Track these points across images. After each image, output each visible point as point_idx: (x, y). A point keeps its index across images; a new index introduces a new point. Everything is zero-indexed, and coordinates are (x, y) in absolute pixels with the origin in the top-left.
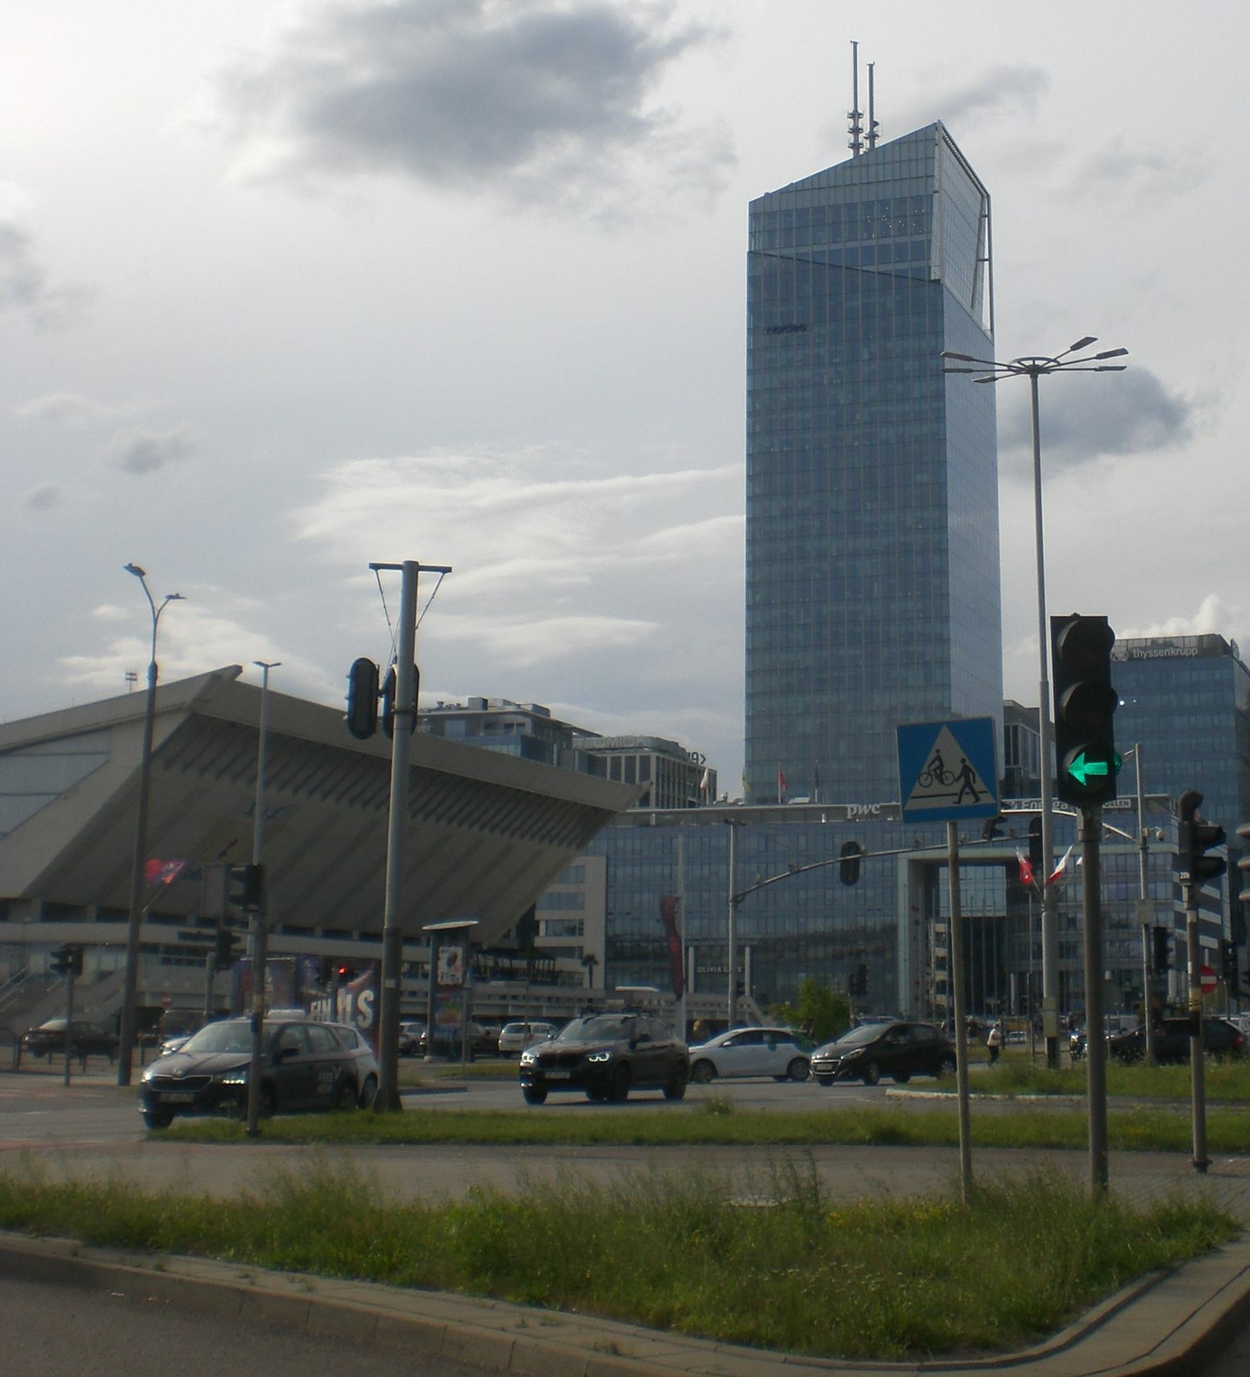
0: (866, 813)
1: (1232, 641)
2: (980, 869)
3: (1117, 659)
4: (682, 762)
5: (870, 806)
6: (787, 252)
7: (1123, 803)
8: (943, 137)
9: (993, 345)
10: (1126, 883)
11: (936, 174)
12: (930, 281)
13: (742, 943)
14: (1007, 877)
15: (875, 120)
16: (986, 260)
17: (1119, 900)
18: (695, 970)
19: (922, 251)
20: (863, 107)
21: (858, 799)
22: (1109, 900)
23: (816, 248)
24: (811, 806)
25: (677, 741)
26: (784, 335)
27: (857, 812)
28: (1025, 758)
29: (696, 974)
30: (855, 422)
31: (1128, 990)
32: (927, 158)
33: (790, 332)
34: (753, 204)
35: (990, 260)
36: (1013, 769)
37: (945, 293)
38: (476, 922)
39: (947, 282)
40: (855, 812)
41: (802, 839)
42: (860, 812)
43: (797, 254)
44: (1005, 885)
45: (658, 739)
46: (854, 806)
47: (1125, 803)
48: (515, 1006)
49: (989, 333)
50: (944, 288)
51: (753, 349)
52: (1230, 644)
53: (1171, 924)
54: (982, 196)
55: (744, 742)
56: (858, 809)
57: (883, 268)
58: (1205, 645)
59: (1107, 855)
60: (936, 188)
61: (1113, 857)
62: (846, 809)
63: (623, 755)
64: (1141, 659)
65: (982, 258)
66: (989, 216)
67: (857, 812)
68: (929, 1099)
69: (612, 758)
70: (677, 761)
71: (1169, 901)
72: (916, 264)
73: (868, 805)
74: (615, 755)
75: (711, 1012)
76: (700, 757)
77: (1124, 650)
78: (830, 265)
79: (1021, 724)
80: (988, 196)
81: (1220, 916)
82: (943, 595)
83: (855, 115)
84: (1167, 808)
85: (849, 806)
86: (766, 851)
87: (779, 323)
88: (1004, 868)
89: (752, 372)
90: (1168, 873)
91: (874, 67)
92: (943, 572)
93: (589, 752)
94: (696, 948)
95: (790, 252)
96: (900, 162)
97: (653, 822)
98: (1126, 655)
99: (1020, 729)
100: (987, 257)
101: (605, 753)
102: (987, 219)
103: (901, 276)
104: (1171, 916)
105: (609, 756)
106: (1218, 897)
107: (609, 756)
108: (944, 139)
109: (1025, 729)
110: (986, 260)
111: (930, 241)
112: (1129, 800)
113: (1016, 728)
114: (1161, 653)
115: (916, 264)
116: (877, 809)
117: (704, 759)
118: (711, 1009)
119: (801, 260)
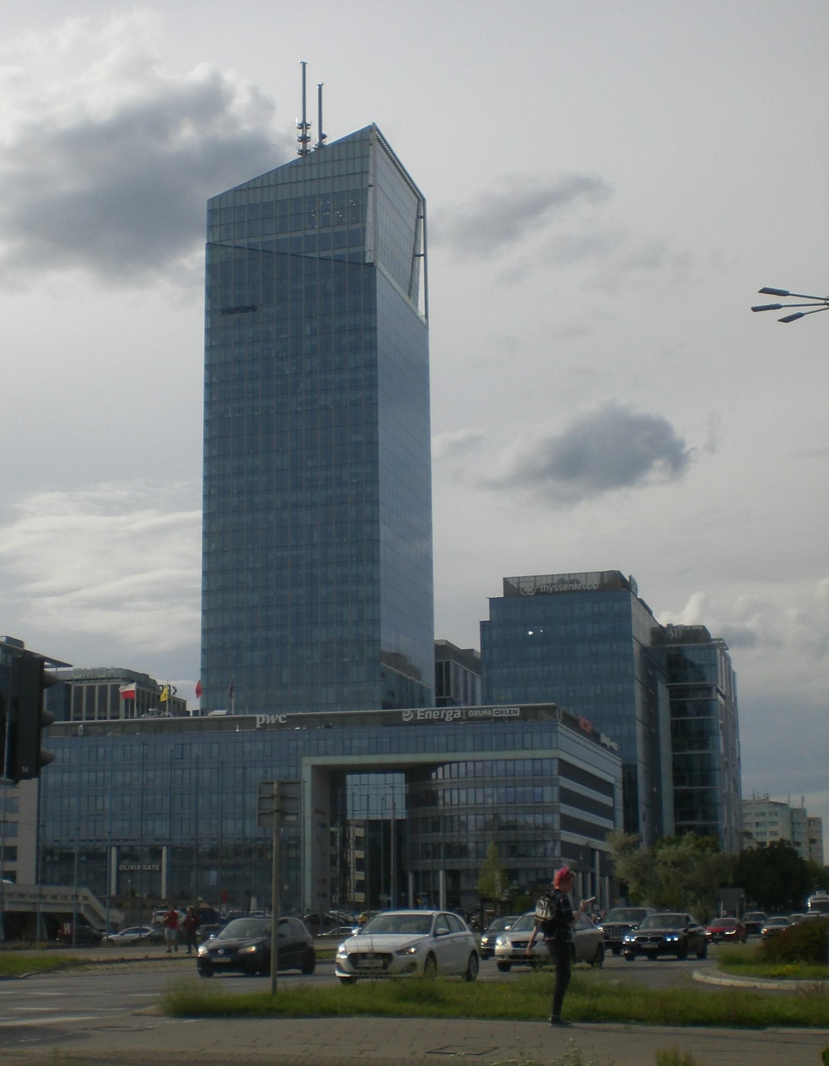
0: (273, 722)
1: (630, 577)
2: (381, 777)
3: (525, 593)
4: (152, 691)
5: (277, 716)
6: (239, 242)
7: (512, 712)
8: (377, 137)
9: (428, 330)
10: (515, 787)
11: (371, 169)
12: (365, 264)
13: (159, 843)
14: (406, 783)
15: (324, 132)
16: (422, 255)
17: (507, 803)
18: (118, 868)
19: (358, 238)
20: (312, 118)
21: (268, 708)
22: (498, 803)
23: (266, 239)
24: (228, 716)
25: (148, 674)
26: (236, 316)
27: (266, 721)
28: (457, 691)
29: (119, 872)
30: (298, 391)
31: (516, 887)
32: (813, 841)
33: (241, 312)
34: (211, 201)
35: (425, 255)
36: (446, 699)
37: (378, 273)
38: (722, 904)
39: (380, 265)
40: (263, 722)
41: (215, 747)
42: (268, 722)
43: (248, 244)
44: (404, 789)
45: (128, 670)
46: (263, 716)
47: (514, 711)
48: (10, 903)
49: (424, 319)
50: (377, 270)
51: (211, 328)
52: (628, 579)
53: (557, 826)
54: (419, 200)
55: (200, 672)
56: (266, 718)
57: (324, 254)
58: (606, 581)
59: (497, 760)
60: (371, 182)
61: (504, 762)
62: (255, 719)
63: (97, 685)
64: (547, 593)
65: (418, 253)
66: (424, 217)
67: (266, 721)
68: (84, 1021)
69: (87, 687)
70: (147, 690)
71: (556, 804)
72: (353, 250)
73: (275, 715)
74: (90, 684)
75: (35, 904)
76: (172, 689)
77: (532, 585)
78: (277, 253)
79: (452, 660)
80: (424, 200)
81: (612, 822)
82: (374, 541)
83: (304, 126)
84: (555, 717)
85: (258, 716)
86: (182, 758)
87: (232, 304)
88: (404, 775)
89: (209, 349)
90: (555, 777)
91: (323, 87)
92: (374, 521)
93: (66, 682)
94: (119, 848)
95: (243, 242)
96: (339, 160)
97: (80, 733)
98: (534, 590)
99: (451, 665)
100: (422, 253)
101: (82, 683)
102: (422, 219)
103: (339, 260)
104: (557, 818)
105: (85, 685)
106: (610, 804)
107: (85, 685)
108: (380, 142)
109: (473, 675)
110: (422, 255)
111: (364, 230)
112: (518, 709)
113: (448, 664)
114: (565, 588)
115: (353, 250)
116: (283, 719)
117: (176, 691)
118: (33, 901)
119: (252, 249)
